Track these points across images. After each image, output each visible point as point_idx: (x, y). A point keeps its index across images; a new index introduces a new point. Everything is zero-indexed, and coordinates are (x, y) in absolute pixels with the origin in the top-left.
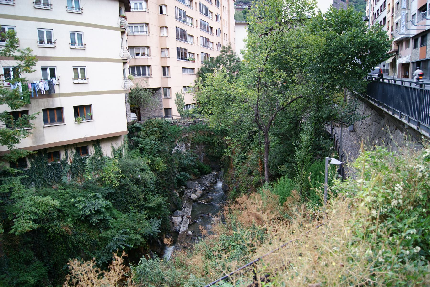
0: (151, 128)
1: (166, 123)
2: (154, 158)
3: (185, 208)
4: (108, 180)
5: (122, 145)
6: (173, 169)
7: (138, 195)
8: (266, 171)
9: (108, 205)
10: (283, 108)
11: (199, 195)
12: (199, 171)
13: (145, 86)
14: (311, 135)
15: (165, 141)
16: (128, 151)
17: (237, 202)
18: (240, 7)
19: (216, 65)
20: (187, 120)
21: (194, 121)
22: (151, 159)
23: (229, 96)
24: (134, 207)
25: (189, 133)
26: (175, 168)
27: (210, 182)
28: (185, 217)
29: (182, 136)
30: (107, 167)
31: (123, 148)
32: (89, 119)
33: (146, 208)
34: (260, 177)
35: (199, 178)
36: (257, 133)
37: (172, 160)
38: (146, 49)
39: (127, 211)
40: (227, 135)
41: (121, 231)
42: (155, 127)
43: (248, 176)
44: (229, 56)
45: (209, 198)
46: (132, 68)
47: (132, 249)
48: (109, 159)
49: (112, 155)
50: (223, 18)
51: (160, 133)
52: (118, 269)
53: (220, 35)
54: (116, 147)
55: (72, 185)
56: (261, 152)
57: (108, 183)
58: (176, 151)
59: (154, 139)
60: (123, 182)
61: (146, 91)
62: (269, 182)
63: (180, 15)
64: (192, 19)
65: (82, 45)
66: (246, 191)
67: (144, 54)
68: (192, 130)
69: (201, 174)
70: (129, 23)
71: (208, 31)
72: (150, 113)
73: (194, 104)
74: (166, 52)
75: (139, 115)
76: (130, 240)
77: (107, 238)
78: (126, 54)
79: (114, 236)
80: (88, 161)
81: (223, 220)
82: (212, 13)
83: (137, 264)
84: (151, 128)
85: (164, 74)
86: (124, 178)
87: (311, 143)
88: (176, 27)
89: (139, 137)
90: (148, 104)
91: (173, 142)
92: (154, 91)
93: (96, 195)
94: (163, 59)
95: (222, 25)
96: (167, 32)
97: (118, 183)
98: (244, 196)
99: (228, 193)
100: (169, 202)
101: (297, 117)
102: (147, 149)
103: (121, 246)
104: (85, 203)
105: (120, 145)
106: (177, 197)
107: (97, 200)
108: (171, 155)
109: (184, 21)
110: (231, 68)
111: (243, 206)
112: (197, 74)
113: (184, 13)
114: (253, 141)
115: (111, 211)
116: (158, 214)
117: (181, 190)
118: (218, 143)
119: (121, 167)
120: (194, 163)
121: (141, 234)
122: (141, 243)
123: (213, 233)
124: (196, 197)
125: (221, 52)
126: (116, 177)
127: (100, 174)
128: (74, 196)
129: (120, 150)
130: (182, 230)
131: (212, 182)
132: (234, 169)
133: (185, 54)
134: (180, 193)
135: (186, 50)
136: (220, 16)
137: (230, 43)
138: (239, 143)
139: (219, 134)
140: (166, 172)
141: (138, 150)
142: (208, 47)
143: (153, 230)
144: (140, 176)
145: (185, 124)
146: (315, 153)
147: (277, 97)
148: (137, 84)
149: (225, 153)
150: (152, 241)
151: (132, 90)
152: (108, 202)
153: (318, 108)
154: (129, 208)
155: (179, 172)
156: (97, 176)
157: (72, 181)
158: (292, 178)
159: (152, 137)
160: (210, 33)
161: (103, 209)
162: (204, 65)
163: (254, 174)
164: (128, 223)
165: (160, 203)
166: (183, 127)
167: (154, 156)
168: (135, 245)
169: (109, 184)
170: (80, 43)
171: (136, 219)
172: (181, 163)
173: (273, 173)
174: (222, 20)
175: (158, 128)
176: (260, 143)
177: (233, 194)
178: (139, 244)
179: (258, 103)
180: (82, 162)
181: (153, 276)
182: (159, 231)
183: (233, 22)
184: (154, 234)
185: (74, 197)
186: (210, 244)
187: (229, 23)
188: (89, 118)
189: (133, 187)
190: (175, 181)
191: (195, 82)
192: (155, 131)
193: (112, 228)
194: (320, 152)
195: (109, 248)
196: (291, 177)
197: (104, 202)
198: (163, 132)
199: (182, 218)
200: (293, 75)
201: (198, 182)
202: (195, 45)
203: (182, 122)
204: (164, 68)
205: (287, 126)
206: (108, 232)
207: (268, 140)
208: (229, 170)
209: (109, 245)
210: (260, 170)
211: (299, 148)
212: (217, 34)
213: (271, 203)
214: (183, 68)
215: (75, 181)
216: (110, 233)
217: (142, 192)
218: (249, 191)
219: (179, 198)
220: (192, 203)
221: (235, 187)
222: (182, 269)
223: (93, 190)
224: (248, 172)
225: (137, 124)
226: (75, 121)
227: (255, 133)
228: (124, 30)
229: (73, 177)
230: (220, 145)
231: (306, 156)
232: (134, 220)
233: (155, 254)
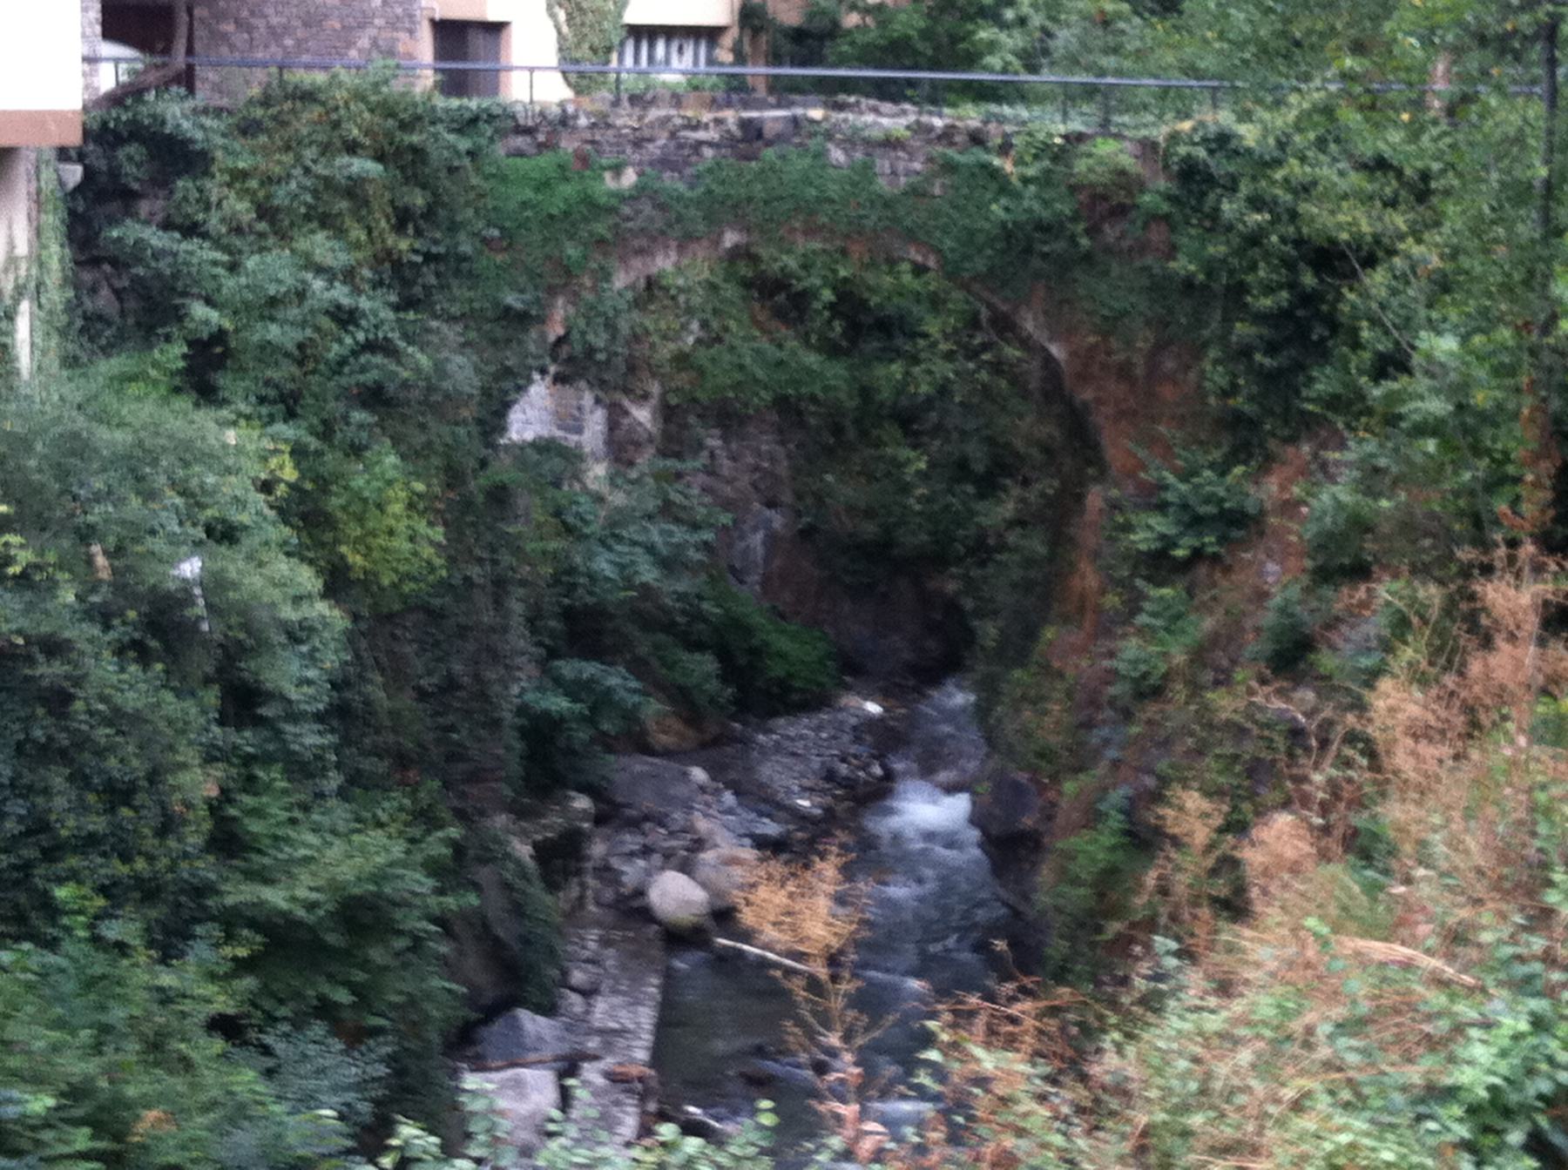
0: (309, 153)
2: (332, 460)
3: (588, 993)
15: (441, 302)
21: (745, 124)
24: (103, 890)
29: (613, 263)
35: (716, 742)
42: (352, 148)
51: (403, 219)
73: (708, 35)
84: (309, 153)
89: (191, 230)
102: (267, 350)
116: (342, 996)
117: (553, 823)
131: (849, 784)
134: (544, 852)
139: (980, 265)
140: (435, 615)
144: (191, 568)
145: (653, 149)
159: (320, 245)
175: (380, 157)
192: (354, 190)
198: (429, 214)
201: (715, 770)
208: (1049, 633)
220: (656, 952)
221: (1118, 795)
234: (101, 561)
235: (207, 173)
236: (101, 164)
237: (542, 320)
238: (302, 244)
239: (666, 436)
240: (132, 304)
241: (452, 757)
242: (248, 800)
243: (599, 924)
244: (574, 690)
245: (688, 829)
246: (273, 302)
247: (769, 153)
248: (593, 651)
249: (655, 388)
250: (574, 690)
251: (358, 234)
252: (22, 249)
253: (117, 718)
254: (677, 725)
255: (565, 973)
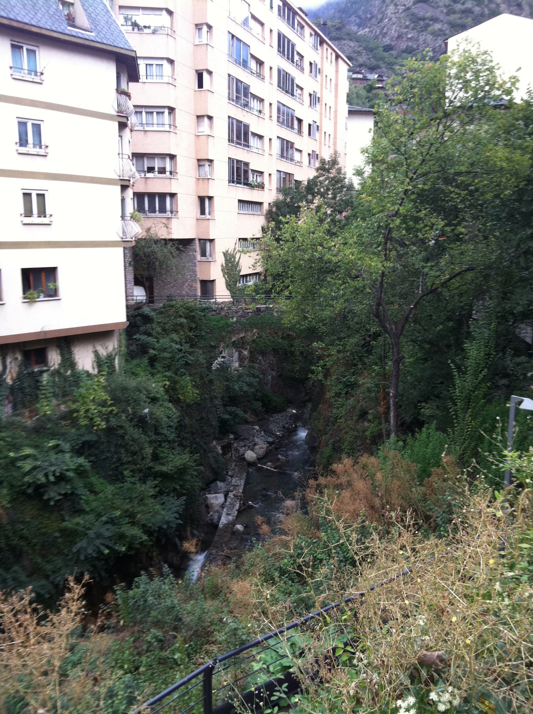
1: (203, 310)
2: (177, 378)
3: (232, 477)
4: (85, 417)
5: (114, 349)
6: (211, 399)
7: (141, 449)
8: (392, 414)
9: (81, 466)
10: (433, 291)
11: (262, 452)
12: (263, 406)
13: (163, 234)
14: (487, 346)
16: (127, 360)
17: (334, 472)
18: (360, 76)
19: (305, 197)
20: (244, 305)
21: (257, 308)
22: (170, 379)
23: (326, 263)
24: (132, 471)
25: (246, 331)
26: (216, 397)
27: (284, 427)
28: (231, 495)
30: (83, 391)
31: (116, 354)
32: (50, 296)
33: (156, 475)
34: (380, 423)
35: (261, 420)
36: (379, 335)
37: (211, 381)
38: (168, 160)
39: (118, 480)
40: (320, 339)
41: (104, 519)
42: (181, 316)
43: (357, 421)
44: (333, 179)
45: (279, 459)
46: (139, 196)
47: (125, 555)
48: (88, 374)
49: (93, 368)
50: (324, 100)
51: (191, 329)
52: (74, 607)
53: (317, 135)
54: (103, 352)
55: (12, 424)
56: (385, 374)
57: (83, 422)
58: (220, 364)
59: (178, 340)
60: (113, 422)
61: (166, 244)
62: (397, 436)
63: (238, 91)
64: (261, 100)
65: (41, 147)
66: (353, 453)
67: (162, 171)
68: (252, 325)
69: (267, 412)
70: (135, 106)
71: (292, 128)
72: (172, 287)
74: (207, 168)
75: (150, 291)
76: (121, 537)
77: (76, 531)
78: (127, 168)
79: (89, 529)
80: (45, 377)
81: (304, 505)
82: (302, 89)
83: (129, 587)
85: (203, 212)
86: (116, 414)
87: (487, 363)
88: (229, 117)
89: (150, 335)
90: (168, 271)
91: (215, 347)
92: (181, 246)
93: (58, 446)
94: (201, 181)
95: (321, 114)
96: (211, 127)
97: (104, 423)
98: (347, 461)
99: (317, 451)
100: (202, 465)
101: (462, 308)
102: (164, 358)
103: (102, 548)
104: (36, 459)
105: (110, 348)
106: (218, 454)
107: (60, 456)
108: (210, 372)
109: (246, 105)
110: (335, 203)
111: (344, 479)
112: (267, 214)
113: (247, 88)
114: (369, 352)
115: (87, 477)
116: (178, 487)
118: (302, 353)
119: (112, 393)
120: (253, 390)
121: (144, 526)
122: (141, 543)
123: (283, 532)
124: (255, 455)
125: (317, 170)
126: (100, 412)
127: (70, 403)
128: (14, 445)
129: (110, 358)
130: (224, 520)
131: (288, 429)
132: (331, 406)
133: (246, 172)
134: (223, 448)
135: (247, 164)
136: (318, 95)
137: (336, 153)
138: (341, 355)
140: (198, 404)
141: (146, 361)
142: (292, 160)
143: (167, 518)
144: (146, 411)
146: (493, 383)
147: (423, 267)
148: (148, 230)
149: (313, 372)
150: (163, 541)
151: (138, 241)
152: (81, 460)
153: (505, 293)
154: (122, 474)
155: (225, 405)
156: (63, 408)
157: (13, 416)
158: (445, 431)
159: (175, 336)
160: (296, 131)
161: (71, 474)
162: (281, 197)
163: (370, 417)
164: (118, 502)
165: (184, 464)
166: (235, 319)
167: (176, 374)
168: (130, 548)
169: (85, 425)
170: (37, 142)
171: (134, 496)
172: (228, 388)
173: (408, 419)
174: (321, 105)
175: (186, 318)
176: (382, 359)
177: (328, 454)
178: (138, 546)
179: (382, 280)
180: (35, 378)
181: (159, 612)
182: (180, 521)
183: (344, 108)
184: (169, 527)
185: (16, 448)
186: (275, 554)
187: (336, 112)
188: (52, 293)
189: (134, 433)
190: (215, 423)
191: (263, 229)
192: (181, 325)
193: (87, 513)
194: (504, 381)
195: (78, 551)
196: (441, 428)
197: (75, 459)
198: (196, 328)
199: (226, 496)
200: (459, 224)
202: (266, 154)
203: (234, 308)
204: (202, 199)
205: (441, 327)
206: (78, 520)
207: (399, 354)
208: (320, 406)
209: (79, 545)
210: (381, 409)
211: (462, 372)
212: (310, 134)
213: (399, 478)
214: (240, 201)
215: (18, 415)
216: (82, 522)
217: (151, 442)
218: (359, 451)
219: (221, 459)
221: (331, 441)
222: (218, 602)
223: (53, 435)
224: (357, 412)
225: (146, 310)
226: (25, 298)
227: (376, 336)
228: (124, 120)
229: (15, 408)
230: (306, 357)
231: (476, 388)
232: (130, 498)
233: (166, 568)
234: (130, 410)
235: (153, 323)
236: (133, 321)
237: (218, 347)
238: (171, 336)
239: (251, 357)
240: (139, 347)
241: (203, 432)
242: (160, 449)
243: (235, 461)
244: (230, 413)
245: (254, 441)
246: (165, 349)
247: (262, 314)
248: (236, 405)
249: (248, 347)
250: (230, 413)
251: (182, 333)
252: (116, 347)
253: (133, 440)
254: (253, 417)
255: (228, 472)
